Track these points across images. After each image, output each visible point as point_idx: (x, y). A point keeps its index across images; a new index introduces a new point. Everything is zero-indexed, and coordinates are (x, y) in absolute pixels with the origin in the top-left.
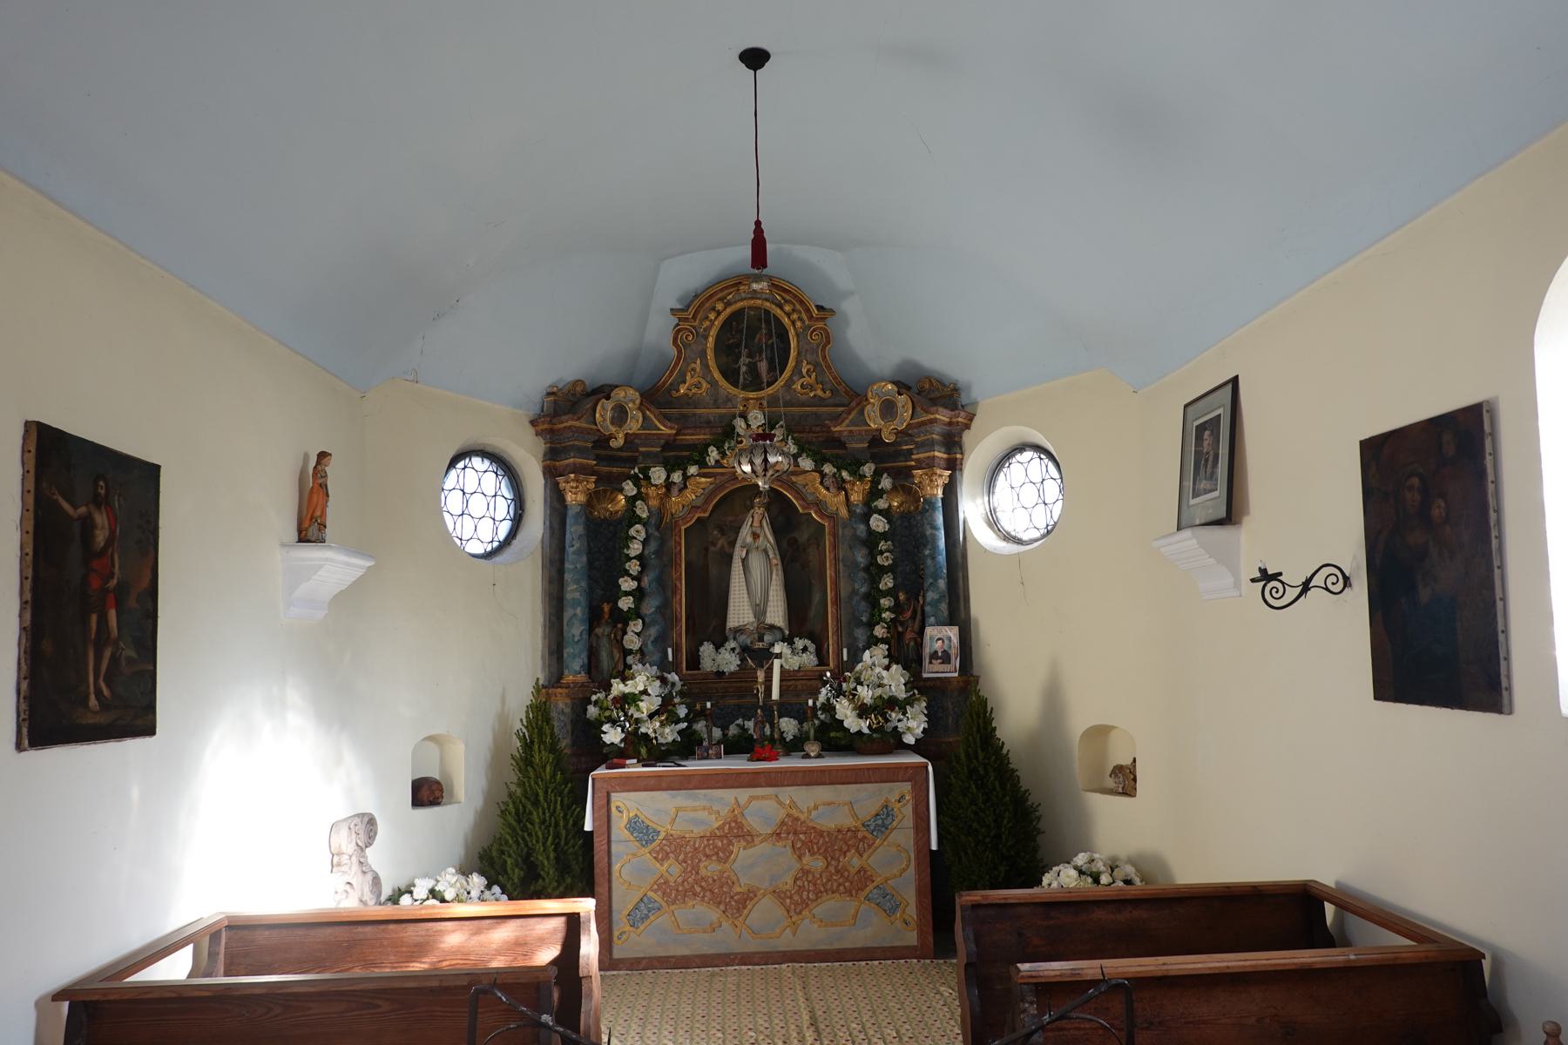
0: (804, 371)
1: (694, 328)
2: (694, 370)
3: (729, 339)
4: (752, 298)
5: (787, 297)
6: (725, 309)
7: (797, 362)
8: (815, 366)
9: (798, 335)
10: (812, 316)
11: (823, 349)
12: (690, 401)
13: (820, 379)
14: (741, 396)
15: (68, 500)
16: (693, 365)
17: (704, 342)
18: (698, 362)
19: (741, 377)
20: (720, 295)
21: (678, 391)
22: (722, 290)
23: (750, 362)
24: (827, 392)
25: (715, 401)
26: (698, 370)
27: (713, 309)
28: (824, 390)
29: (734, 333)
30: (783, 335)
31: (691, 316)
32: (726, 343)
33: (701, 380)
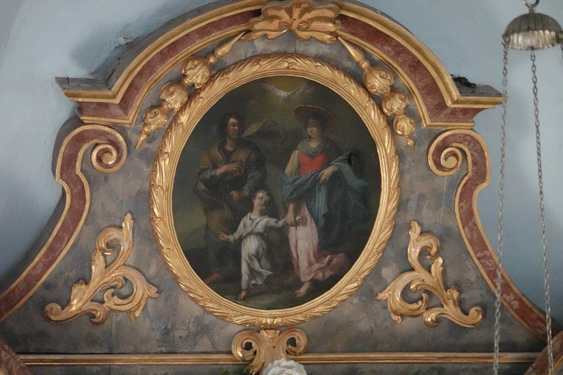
0: (413, 252)
1: (122, 130)
2: (113, 246)
3: (215, 166)
4: (284, 55)
5: (377, 53)
6: (211, 79)
7: (395, 227)
8: (441, 240)
9: (400, 154)
10: (445, 106)
11: (467, 195)
12: (97, 332)
13: (452, 276)
14: (239, 320)
15: (41, 277)
16: (114, 234)
17: (147, 170)
18: (128, 224)
19: (244, 267)
20: (197, 45)
21: (66, 303)
22: (203, 32)
23: (268, 228)
24: (473, 311)
25: (167, 332)
26: (125, 246)
27: (179, 81)
28: (460, 304)
29: (229, 148)
30: (403, 293)
31: (117, 101)
32: (208, 174)
33: (132, 274)
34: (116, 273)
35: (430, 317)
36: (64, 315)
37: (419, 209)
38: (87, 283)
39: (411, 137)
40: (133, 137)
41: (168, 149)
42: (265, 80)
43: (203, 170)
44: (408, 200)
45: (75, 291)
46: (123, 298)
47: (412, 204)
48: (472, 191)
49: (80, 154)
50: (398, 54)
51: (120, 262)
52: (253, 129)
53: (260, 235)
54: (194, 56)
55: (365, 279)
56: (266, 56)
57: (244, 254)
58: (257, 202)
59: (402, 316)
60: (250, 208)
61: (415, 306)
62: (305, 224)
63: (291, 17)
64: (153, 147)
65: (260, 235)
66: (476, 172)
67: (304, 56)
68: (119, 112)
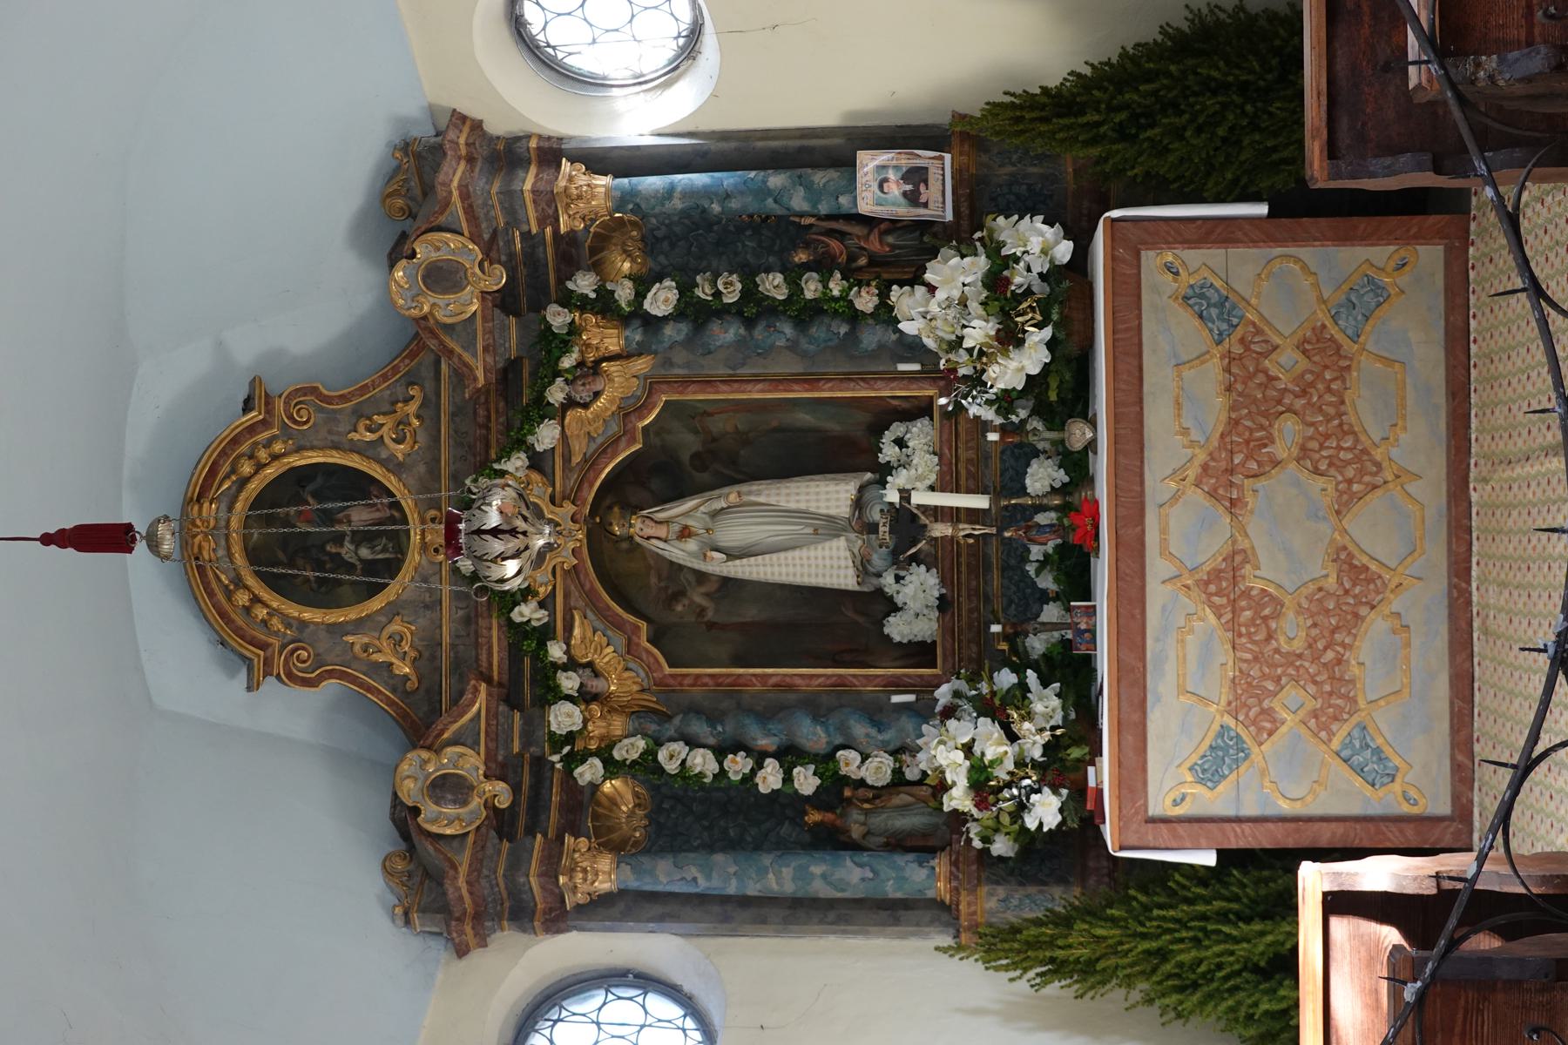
0: (369, 437)
1: (284, 647)
2: (365, 648)
4: (227, 537)
5: (226, 468)
6: (247, 588)
9: (299, 449)
11: (328, 400)
12: (426, 654)
14: (417, 557)
16: (357, 648)
17: (312, 627)
18: (350, 639)
19: (380, 556)
20: (221, 597)
21: (406, 678)
22: (211, 594)
23: (352, 542)
25: (427, 607)
26: (366, 640)
27: (247, 610)
28: (408, 400)
31: (262, 653)
33: (385, 634)
34: (385, 644)
35: (416, 423)
36: (414, 678)
37: (339, 434)
38: (392, 664)
39: (285, 442)
40: (289, 638)
41: (296, 614)
42: (246, 549)
43: (312, 589)
44: (332, 441)
45: (397, 672)
46: (402, 639)
47: (336, 438)
48: (325, 396)
49: (301, 674)
50: (226, 454)
51: (377, 642)
52: (281, 556)
53: (357, 548)
54: (229, 599)
55: (388, 470)
56: (228, 548)
57: (370, 557)
58: (334, 550)
59: (415, 442)
60: (339, 554)
61: (408, 434)
62: (349, 516)
63: (198, 534)
64: (295, 624)
65: (357, 546)
66: (312, 394)
67: (228, 522)
68: (270, 650)
